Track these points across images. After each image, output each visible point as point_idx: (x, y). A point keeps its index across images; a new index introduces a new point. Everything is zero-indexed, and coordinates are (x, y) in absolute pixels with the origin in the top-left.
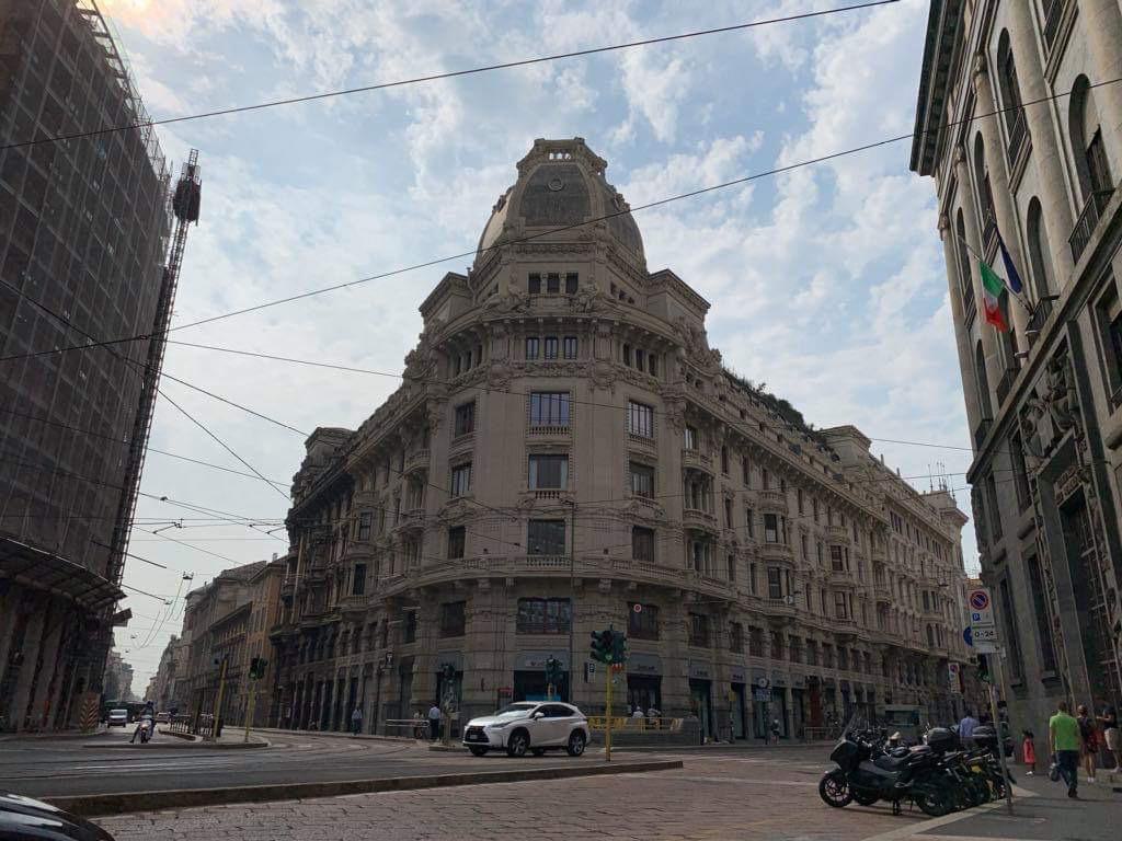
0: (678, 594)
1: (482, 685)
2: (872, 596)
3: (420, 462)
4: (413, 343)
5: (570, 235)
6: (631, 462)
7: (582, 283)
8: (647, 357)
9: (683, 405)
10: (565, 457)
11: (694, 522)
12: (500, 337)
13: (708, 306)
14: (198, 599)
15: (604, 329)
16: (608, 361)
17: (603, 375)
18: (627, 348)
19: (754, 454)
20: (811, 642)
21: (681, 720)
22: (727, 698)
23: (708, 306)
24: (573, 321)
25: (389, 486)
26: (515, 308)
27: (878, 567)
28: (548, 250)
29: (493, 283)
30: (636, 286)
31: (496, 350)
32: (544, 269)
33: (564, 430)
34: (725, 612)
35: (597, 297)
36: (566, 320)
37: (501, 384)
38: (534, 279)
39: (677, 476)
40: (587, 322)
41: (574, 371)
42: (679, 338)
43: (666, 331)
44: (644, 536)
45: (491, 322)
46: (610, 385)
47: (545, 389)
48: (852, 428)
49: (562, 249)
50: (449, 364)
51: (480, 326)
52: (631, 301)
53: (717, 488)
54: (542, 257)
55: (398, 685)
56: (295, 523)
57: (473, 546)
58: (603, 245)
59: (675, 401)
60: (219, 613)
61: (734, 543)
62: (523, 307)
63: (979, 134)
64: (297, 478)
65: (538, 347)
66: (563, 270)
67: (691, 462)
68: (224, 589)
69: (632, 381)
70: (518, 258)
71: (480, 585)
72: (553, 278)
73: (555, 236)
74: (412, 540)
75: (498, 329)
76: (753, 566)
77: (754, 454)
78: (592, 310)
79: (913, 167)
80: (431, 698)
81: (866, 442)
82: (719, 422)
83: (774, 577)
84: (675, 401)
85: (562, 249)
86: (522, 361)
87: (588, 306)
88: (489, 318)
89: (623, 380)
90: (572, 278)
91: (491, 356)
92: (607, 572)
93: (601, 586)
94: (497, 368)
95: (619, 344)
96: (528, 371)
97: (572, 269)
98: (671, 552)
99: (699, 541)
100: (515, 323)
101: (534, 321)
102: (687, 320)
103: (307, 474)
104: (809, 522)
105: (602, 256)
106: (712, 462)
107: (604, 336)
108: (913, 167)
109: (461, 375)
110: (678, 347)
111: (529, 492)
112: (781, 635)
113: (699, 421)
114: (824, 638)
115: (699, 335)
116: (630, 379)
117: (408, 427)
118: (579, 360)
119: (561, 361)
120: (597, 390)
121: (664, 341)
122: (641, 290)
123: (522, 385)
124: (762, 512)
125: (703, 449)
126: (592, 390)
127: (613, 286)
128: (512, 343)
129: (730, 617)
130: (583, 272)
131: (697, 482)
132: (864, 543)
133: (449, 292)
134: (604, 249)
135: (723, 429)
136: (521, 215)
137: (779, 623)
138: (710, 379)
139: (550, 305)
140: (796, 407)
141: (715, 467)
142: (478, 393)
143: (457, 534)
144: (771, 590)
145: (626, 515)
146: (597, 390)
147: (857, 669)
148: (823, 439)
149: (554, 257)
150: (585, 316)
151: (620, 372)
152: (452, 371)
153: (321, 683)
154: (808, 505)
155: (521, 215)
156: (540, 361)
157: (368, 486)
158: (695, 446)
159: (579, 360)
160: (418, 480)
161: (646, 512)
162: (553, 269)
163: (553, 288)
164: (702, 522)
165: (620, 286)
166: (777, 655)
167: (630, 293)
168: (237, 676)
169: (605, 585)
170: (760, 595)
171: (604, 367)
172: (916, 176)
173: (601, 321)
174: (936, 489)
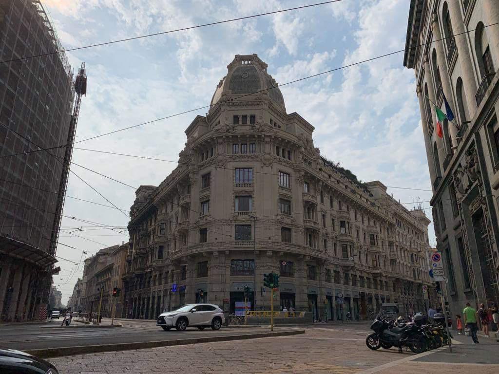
0: (302, 257)
1: (216, 298)
3: (186, 200)
4: (182, 147)
5: (251, 98)
7: (258, 120)
9: (303, 173)
10: (251, 197)
11: (309, 225)
13: (314, 128)
14: (89, 262)
15: (268, 139)
16: (269, 154)
17: (268, 160)
18: (277, 148)
19: (334, 194)
20: (361, 277)
21: (304, 312)
23: (314, 128)
25: (173, 211)
27: (391, 243)
28: (242, 104)
30: (281, 120)
31: (220, 150)
32: (240, 113)
33: (251, 185)
34: (323, 264)
35: (264, 125)
37: (222, 165)
38: (236, 118)
40: (259, 136)
42: (301, 143)
44: (286, 231)
45: (217, 137)
46: (270, 164)
48: (378, 182)
49: (248, 104)
52: (279, 127)
53: (319, 210)
54: (239, 108)
56: (133, 228)
57: (210, 237)
58: (267, 102)
59: (299, 171)
60: (99, 268)
61: (327, 234)
64: (132, 208)
66: (249, 113)
68: (101, 257)
69: (280, 163)
70: (228, 108)
72: (245, 117)
74: (184, 235)
75: (220, 140)
77: (334, 194)
81: (385, 188)
83: (345, 249)
84: (299, 171)
85: (248, 104)
87: (260, 130)
88: (216, 135)
90: (253, 117)
91: (217, 152)
94: (220, 157)
95: (274, 146)
97: (253, 113)
98: (299, 238)
99: (311, 233)
100: (228, 137)
102: (305, 135)
105: (266, 107)
107: (267, 143)
108: (405, 65)
111: (235, 213)
113: (310, 180)
114: (367, 276)
115: (310, 142)
116: (279, 162)
117: (180, 184)
118: (257, 153)
119: (248, 154)
120: (264, 167)
121: (295, 144)
123: (231, 165)
124: (339, 220)
125: (312, 192)
126: (262, 167)
127: (271, 121)
129: (325, 266)
130: (257, 114)
131: (310, 207)
134: (266, 104)
135: (321, 183)
138: (315, 161)
139: (243, 129)
141: (318, 200)
142: (212, 169)
143: (203, 232)
145: (278, 222)
146: (264, 167)
148: (366, 187)
151: (275, 159)
155: (230, 89)
158: (309, 191)
159: (257, 153)
160: (186, 208)
162: (244, 113)
163: (244, 122)
164: (312, 224)
167: (279, 123)
171: (267, 157)
172: (406, 68)
174: (417, 208)
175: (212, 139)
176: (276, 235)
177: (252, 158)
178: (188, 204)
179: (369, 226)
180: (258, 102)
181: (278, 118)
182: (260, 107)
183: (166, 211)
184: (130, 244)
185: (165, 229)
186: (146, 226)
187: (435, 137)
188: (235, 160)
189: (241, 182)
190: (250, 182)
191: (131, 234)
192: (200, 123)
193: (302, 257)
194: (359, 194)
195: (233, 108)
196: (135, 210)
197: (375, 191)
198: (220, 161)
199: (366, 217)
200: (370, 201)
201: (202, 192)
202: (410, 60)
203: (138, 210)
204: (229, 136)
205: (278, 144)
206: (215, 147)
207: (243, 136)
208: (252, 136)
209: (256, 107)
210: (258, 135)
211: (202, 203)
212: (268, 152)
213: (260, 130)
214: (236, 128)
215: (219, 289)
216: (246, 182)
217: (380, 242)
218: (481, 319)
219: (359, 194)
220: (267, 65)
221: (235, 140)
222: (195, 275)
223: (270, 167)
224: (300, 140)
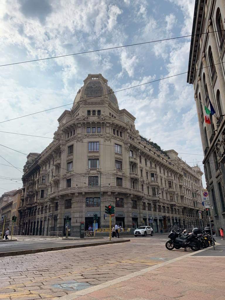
0: (129, 195)
1: (77, 221)
2: (179, 194)
3: (58, 162)
5: (98, 100)
6: (116, 160)
7: (102, 113)
8: (116, 131)
9: (129, 145)
10: (98, 159)
11: (132, 176)
12: (80, 127)
15: (108, 125)
16: (109, 133)
18: (114, 130)
19: (148, 157)
20: (164, 207)
21: (130, 229)
23: (135, 118)
24: (100, 123)
25: (50, 169)
26: (84, 119)
27: (181, 186)
28: (92, 104)
30: (116, 113)
31: (79, 131)
32: (91, 109)
33: (98, 152)
34: (141, 199)
37: (80, 140)
38: (89, 112)
39: (128, 163)
40: (103, 123)
41: (100, 136)
42: (128, 127)
43: (124, 125)
45: (77, 123)
46: (81, 140)
49: (96, 103)
52: (115, 117)
55: (53, 223)
56: (25, 179)
58: (107, 102)
59: (127, 144)
61: (143, 181)
65: (90, 130)
66: (97, 109)
67: (132, 160)
69: (116, 139)
70: (84, 106)
72: (94, 111)
73: (94, 100)
74: (57, 183)
75: (79, 125)
77: (148, 157)
78: (105, 120)
81: (177, 154)
82: (138, 149)
83: (154, 190)
84: (127, 144)
87: (103, 119)
89: (113, 139)
90: (99, 111)
93: (108, 194)
94: (79, 136)
96: (88, 137)
97: (99, 109)
98: (127, 184)
99: (134, 181)
100: (84, 123)
102: (130, 122)
103: (27, 165)
104: (162, 175)
105: (107, 105)
106: (137, 160)
107: (108, 127)
108: (188, 82)
109: (69, 138)
110: (128, 129)
113: (133, 149)
115: (133, 126)
116: (115, 138)
118: (101, 133)
119: (97, 134)
121: (124, 128)
122: (118, 114)
123: (86, 140)
126: (105, 141)
127: (110, 114)
128: (83, 128)
130: (102, 110)
131: (133, 165)
132: (177, 180)
133: (66, 115)
135: (140, 151)
139: (93, 119)
143: (69, 181)
148: (165, 153)
149: (94, 106)
150: (103, 121)
153: (32, 223)
155: (85, 94)
156: (91, 134)
157: (44, 168)
158: (133, 156)
159: (101, 133)
160: (58, 167)
162: (94, 109)
163: (94, 114)
165: (112, 113)
167: (115, 115)
168: (9, 222)
171: (108, 135)
173: (107, 123)
174: (195, 166)
175: (74, 124)
176: (113, 182)
178: (59, 164)
179: (168, 176)
180: (102, 103)
181: (114, 112)
182: (103, 106)
184: (24, 189)
186: (33, 178)
188: (89, 137)
190: (98, 150)
191: (24, 183)
193: (129, 195)
194: (162, 157)
195: (87, 106)
196: (26, 168)
197: (172, 156)
198: (79, 138)
200: (168, 162)
203: (28, 168)
205: (87, 126)
206: (76, 129)
207: (93, 123)
208: (99, 123)
209: (101, 106)
211: (68, 163)
212: (108, 132)
213: (103, 119)
215: (78, 216)
216: (95, 150)
219: (162, 157)
221: (88, 125)
222: (63, 207)
223: (110, 141)
224: (127, 125)
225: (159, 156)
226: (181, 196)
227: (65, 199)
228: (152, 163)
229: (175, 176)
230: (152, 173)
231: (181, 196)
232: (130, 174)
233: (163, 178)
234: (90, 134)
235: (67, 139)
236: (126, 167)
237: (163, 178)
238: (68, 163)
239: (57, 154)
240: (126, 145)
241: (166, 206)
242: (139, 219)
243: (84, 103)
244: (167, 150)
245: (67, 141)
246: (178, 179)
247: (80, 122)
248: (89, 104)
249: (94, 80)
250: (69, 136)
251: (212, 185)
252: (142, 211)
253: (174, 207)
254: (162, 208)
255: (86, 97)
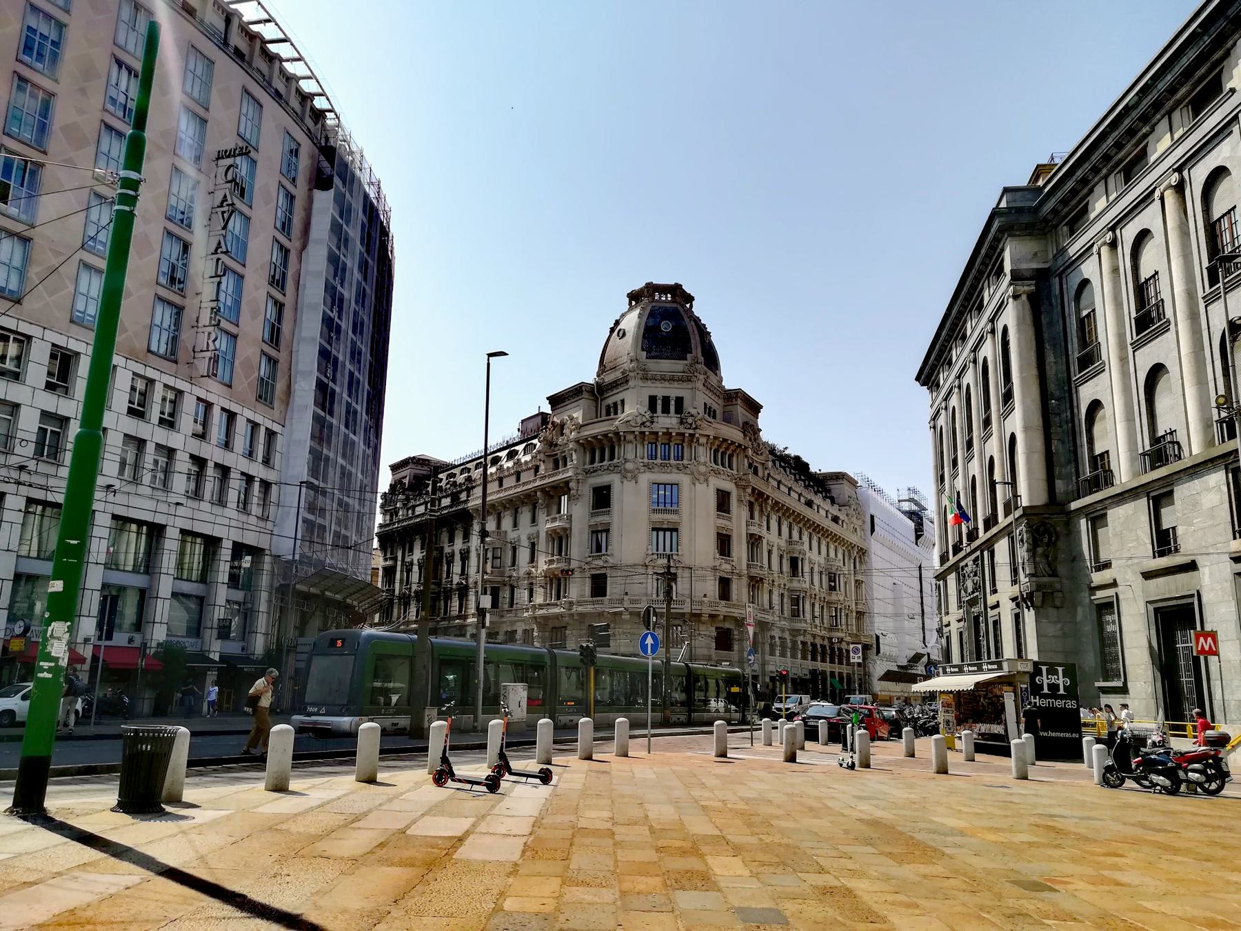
6: (718, 534)
7: (686, 403)
13: (762, 407)
15: (703, 440)
18: (716, 451)
20: (814, 645)
21: (763, 703)
22: (767, 687)
23: (762, 407)
26: (643, 424)
29: (617, 398)
33: (676, 512)
36: (678, 434)
38: (653, 400)
40: (692, 435)
44: (725, 585)
45: (624, 432)
46: (635, 478)
47: (668, 482)
50: (585, 452)
51: (617, 434)
57: (613, 589)
59: (744, 489)
62: (648, 424)
63: (954, 407)
70: (640, 383)
71: (623, 617)
72: (666, 400)
76: (782, 595)
79: (917, 379)
80: (524, 694)
83: (795, 601)
86: (646, 460)
90: (679, 401)
92: (706, 610)
93: (703, 618)
97: (680, 393)
101: (656, 433)
107: (630, 442)
108: (917, 379)
109: (596, 465)
112: (796, 641)
116: (717, 473)
120: (697, 484)
123: (645, 478)
132: (849, 566)
136: (643, 350)
137: (795, 633)
139: (667, 422)
140: (805, 459)
141: (764, 532)
142: (614, 479)
144: (793, 610)
145: (714, 569)
146: (697, 484)
147: (823, 661)
150: (691, 431)
152: (588, 459)
154: (805, 538)
155: (643, 350)
159: (685, 462)
161: (727, 567)
163: (666, 410)
166: (783, 655)
169: (705, 618)
170: (786, 615)
176: (711, 588)
177: (678, 469)
179: (790, 541)
183: (499, 526)
185: (500, 558)
187: (946, 502)
189: (661, 507)
190: (675, 507)
192: (585, 395)
194: (775, 479)
199: (785, 522)
201: (593, 515)
202: (927, 376)
204: (644, 432)
206: (620, 446)
210: (690, 434)
214: (655, 419)
217: (807, 569)
218: (385, 222)
219: (775, 479)
220: (676, 284)
223: (634, 481)
225: (809, 504)
226: (857, 612)
227: (551, 624)
228: (794, 525)
229: (757, 508)
230: (795, 555)
231: (857, 612)
232: (749, 566)
233: (775, 545)
234: (655, 462)
235: (588, 466)
236: (740, 549)
237: (775, 545)
238: (653, 529)
239: (552, 497)
240: (741, 490)
241: (818, 641)
242: (760, 677)
243: (640, 376)
244: (827, 469)
245: (587, 472)
246: (765, 518)
247: (633, 429)
248: (654, 379)
249: (660, 301)
250: (597, 459)
251: (996, 611)
252: (768, 657)
253: (801, 638)
254: (800, 646)
255: (647, 358)
